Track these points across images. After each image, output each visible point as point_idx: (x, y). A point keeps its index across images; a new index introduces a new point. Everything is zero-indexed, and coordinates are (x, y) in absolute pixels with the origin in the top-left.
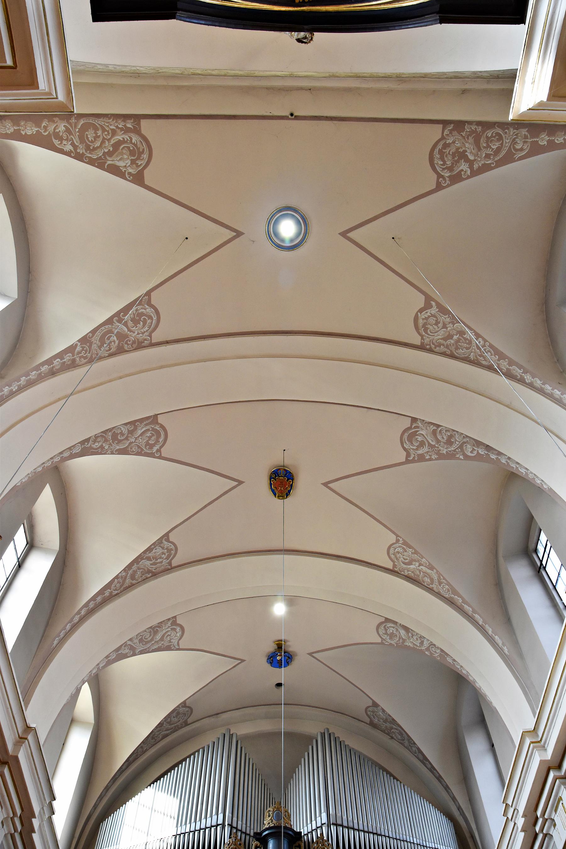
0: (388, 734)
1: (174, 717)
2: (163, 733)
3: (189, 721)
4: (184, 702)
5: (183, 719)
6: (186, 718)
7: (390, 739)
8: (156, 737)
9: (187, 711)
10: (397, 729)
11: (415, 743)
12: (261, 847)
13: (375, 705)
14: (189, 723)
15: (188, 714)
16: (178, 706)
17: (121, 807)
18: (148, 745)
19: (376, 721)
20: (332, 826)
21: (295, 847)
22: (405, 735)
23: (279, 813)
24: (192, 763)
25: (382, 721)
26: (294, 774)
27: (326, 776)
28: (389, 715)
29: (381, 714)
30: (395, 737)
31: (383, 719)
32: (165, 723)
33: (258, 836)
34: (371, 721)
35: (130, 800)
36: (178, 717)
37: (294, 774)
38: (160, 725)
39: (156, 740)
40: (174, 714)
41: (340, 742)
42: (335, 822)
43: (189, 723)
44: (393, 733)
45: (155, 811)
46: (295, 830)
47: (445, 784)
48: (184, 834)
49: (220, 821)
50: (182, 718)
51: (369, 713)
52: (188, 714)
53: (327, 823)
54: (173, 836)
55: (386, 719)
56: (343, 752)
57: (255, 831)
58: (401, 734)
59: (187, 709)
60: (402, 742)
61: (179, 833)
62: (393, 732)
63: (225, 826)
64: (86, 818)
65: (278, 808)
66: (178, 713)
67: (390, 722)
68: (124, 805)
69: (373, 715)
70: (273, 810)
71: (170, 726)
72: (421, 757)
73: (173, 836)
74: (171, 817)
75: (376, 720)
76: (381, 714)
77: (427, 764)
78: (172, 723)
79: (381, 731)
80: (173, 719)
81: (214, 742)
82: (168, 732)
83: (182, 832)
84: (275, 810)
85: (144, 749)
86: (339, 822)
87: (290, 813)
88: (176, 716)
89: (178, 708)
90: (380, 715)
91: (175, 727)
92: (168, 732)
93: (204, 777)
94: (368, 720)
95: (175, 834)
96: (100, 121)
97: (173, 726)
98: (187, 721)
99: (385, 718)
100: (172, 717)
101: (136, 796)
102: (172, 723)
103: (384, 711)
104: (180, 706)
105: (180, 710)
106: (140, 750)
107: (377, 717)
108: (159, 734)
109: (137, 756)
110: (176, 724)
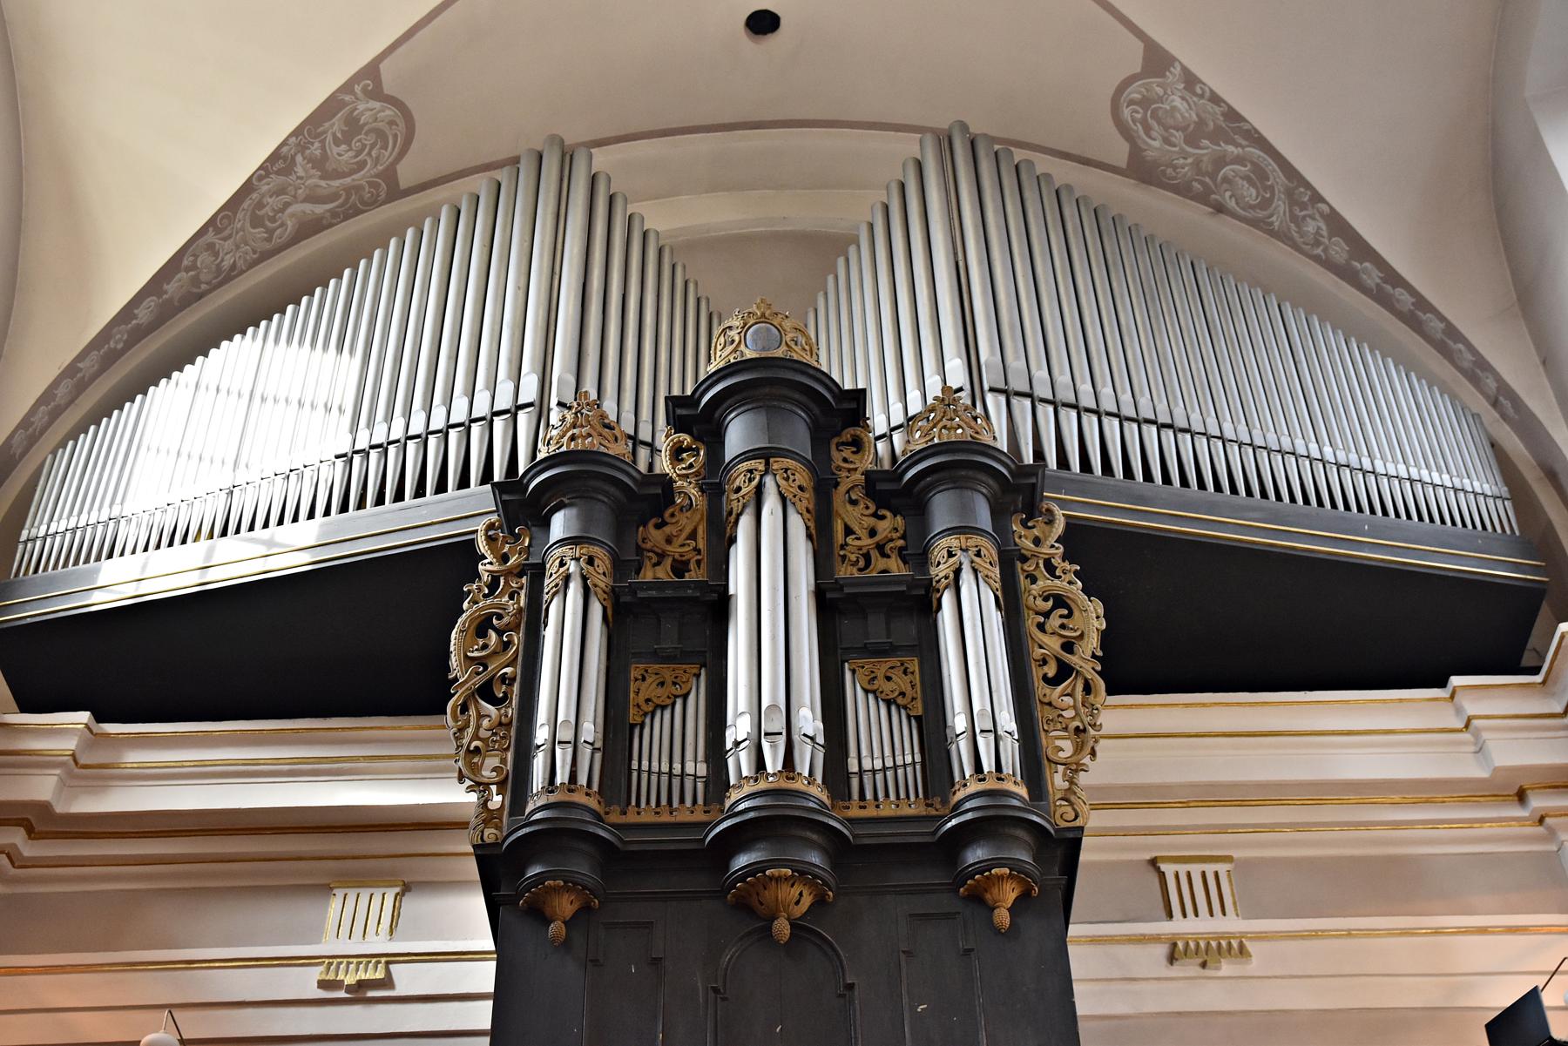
0: (1203, 198)
1: (337, 142)
2: (296, 208)
3: (407, 173)
4: (372, 70)
5: (377, 158)
6: (388, 156)
7: (1212, 213)
8: (273, 220)
9: (392, 123)
10: (1239, 160)
11: (1317, 198)
12: (697, 450)
13: (1157, 60)
14: (403, 184)
15: (395, 136)
16: (347, 87)
17: (128, 405)
18: (238, 247)
19: (1154, 146)
20: (990, 398)
21: (838, 445)
22: (1278, 178)
23: (768, 329)
24: (410, 262)
25: (1178, 137)
26: (831, 279)
27: (961, 264)
28: (1216, 99)
29: (1178, 102)
30: (1232, 204)
31: (1184, 129)
32: (299, 158)
33: (684, 412)
34: (1136, 153)
35: (164, 381)
36: (356, 145)
37: (831, 279)
38: (280, 164)
39: (271, 232)
40: (336, 125)
41: (1017, 167)
42: (1002, 386)
43: (403, 184)
44: (1225, 186)
45: (263, 399)
46: (835, 376)
47: (1442, 326)
48: (383, 448)
49: (529, 392)
50: (374, 153)
51: (1126, 113)
52: (395, 136)
53: (967, 387)
54: (337, 457)
55: (1201, 122)
56: (1027, 194)
57: (676, 392)
58: (1259, 176)
59: (388, 112)
60: (1261, 214)
61: (362, 444)
62: (1226, 180)
63: (549, 410)
64: (11, 502)
65: (763, 315)
66: (353, 126)
67: (1217, 136)
68: (139, 397)
69: (1144, 123)
70: (745, 324)
71: (323, 183)
72: (1339, 250)
73: (337, 457)
74: (328, 409)
75: (1156, 144)
76: (1178, 102)
77: (1365, 271)
78: (330, 166)
79: (1176, 190)
80: (336, 150)
81: (499, 185)
82: (320, 209)
83: (373, 443)
84: (752, 322)
85: (227, 264)
86: (1018, 383)
87: (813, 336)
88: (347, 138)
89: (347, 98)
90: (1174, 108)
91: (348, 190)
92: (320, 209)
93: (458, 294)
94: (1119, 152)
95: (345, 448)
96: (245, 215)
97: (336, 183)
98: (395, 171)
99: (1195, 118)
100: (329, 138)
101: (188, 367)
102: (330, 166)
103: (1190, 80)
104: (358, 89)
105: (361, 107)
106: (205, 258)
107: (1159, 123)
108: (282, 211)
109: (196, 281)
110: (348, 180)
